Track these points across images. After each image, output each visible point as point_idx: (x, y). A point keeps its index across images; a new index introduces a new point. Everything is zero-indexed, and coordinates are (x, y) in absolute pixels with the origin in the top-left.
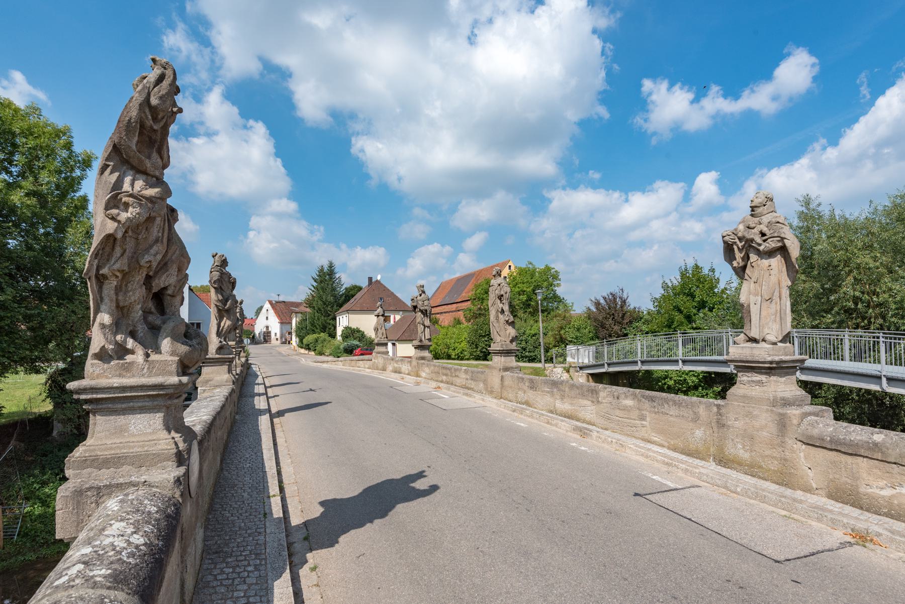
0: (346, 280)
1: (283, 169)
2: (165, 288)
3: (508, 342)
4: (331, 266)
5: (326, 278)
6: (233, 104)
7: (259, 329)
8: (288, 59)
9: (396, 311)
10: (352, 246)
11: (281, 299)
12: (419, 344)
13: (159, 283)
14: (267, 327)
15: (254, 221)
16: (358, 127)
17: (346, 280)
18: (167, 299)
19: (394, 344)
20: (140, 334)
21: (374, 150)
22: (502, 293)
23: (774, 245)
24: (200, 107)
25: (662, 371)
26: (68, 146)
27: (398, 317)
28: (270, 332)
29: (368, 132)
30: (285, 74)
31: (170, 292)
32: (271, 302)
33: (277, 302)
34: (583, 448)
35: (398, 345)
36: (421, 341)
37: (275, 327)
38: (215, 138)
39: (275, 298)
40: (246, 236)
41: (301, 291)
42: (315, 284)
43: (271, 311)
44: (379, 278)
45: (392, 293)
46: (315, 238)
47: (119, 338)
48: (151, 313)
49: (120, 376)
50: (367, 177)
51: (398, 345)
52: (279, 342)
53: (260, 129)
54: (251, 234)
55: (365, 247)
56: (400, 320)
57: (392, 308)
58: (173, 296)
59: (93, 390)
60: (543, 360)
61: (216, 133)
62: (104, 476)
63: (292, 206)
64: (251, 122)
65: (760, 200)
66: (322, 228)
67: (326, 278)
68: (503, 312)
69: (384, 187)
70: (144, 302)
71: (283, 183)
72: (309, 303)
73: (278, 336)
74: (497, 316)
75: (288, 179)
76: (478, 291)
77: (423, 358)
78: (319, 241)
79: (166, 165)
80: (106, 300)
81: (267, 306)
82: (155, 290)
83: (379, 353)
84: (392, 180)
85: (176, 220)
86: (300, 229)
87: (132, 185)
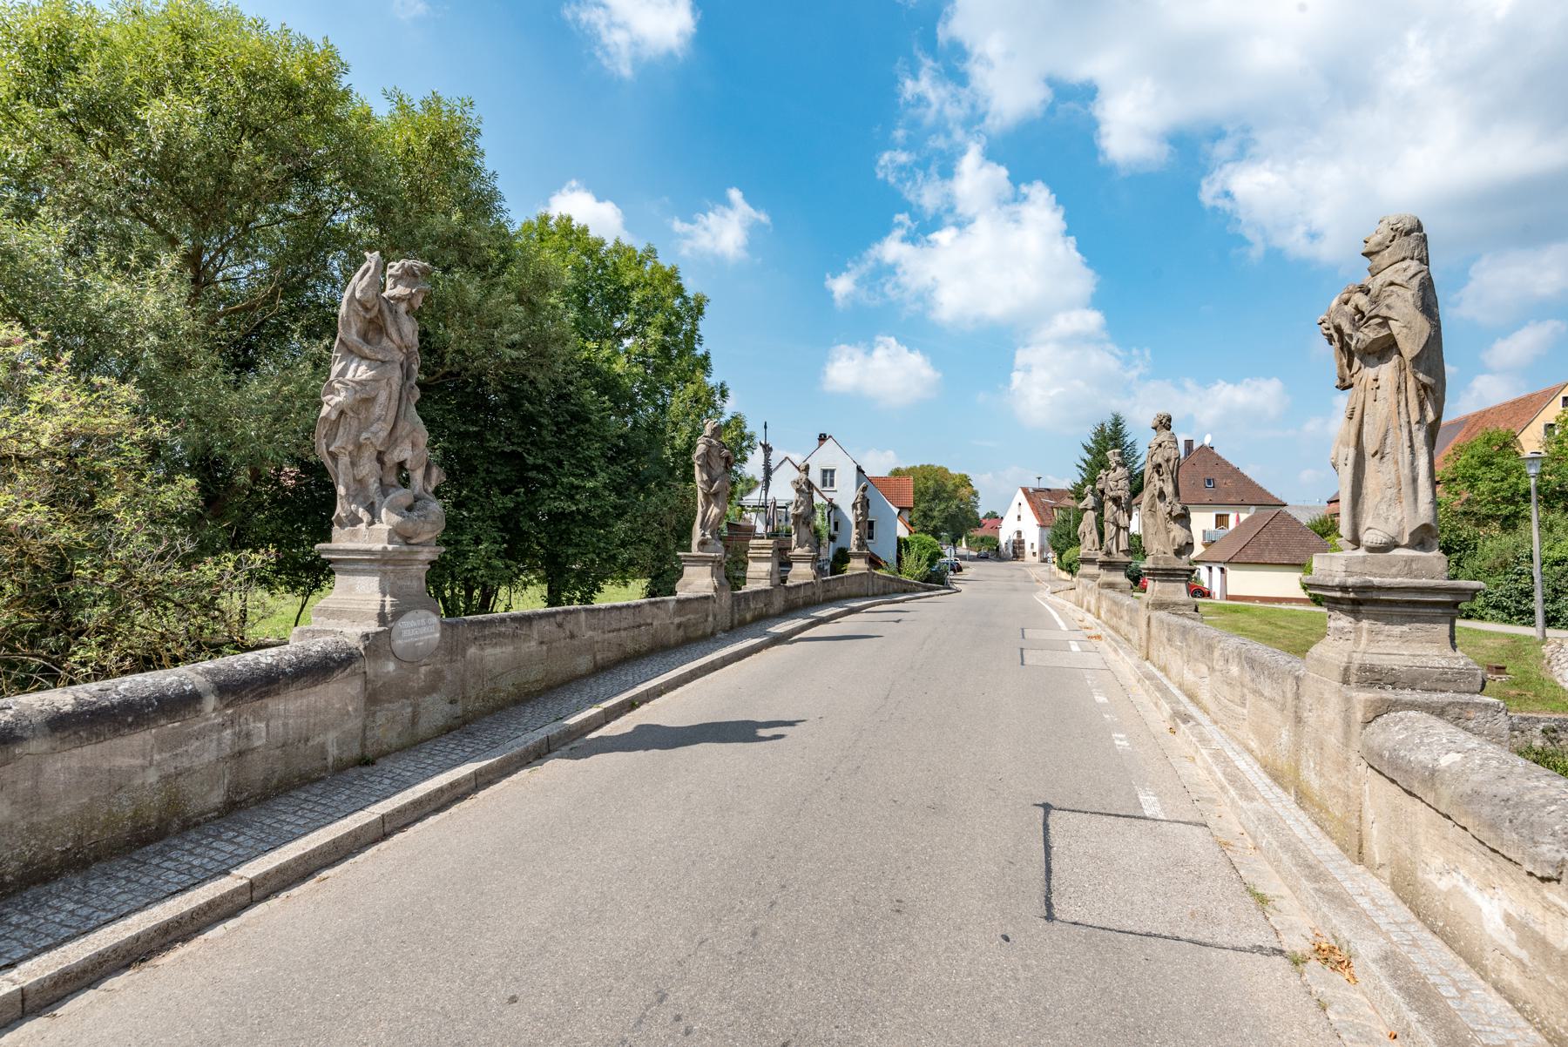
1: (1078, 255)
3: (1171, 554)
4: (1117, 422)
6: (999, 163)
7: (1005, 535)
8: (1096, 65)
9: (1242, 505)
10: (1206, 381)
11: (1043, 485)
12: (1105, 559)
14: (1019, 533)
15: (1022, 357)
16: (1223, 149)
19: (1222, 570)
21: (1252, 185)
22: (1160, 460)
23: (1372, 336)
24: (947, 182)
26: (679, 291)
27: (1244, 517)
28: (1022, 542)
29: (1242, 154)
30: (1088, 92)
32: (1025, 491)
33: (1036, 491)
35: (1230, 572)
36: (1109, 553)
37: (1032, 534)
38: (969, 228)
39: (1033, 484)
40: (1008, 381)
42: (1088, 457)
43: (1026, 506)
44: (1207, 441)
45: (1236, 470)
46: (1134, 373)
47: (353, 507)
50: (1242, 241)
51: (1230, 572)
52: (1037, 558)
53: (1040, 193)
54: (1017, 377)
55: (1235, 380)
56: (1247, 521)
57: (1232, 500)
60: (1539, 617)
61: (972, 221)
63: (1094, 319)
64: (1024, 189)
65: (1378, 238)
66: (1147, 353)
67: (1109, 441)
68: (1162, 495)
69: (1275, 256)
71: (1082, 282)
73: (1036, 549)
74: (1153, 505)
75: (1090, 273)
76: (1462, 461)
77: (1111, 586)
78: (1140, 377)
81: (1021, 497)
83: (1085, 576)
84: (1294, 243)
86: (1102, 360)
87: (356, 371)
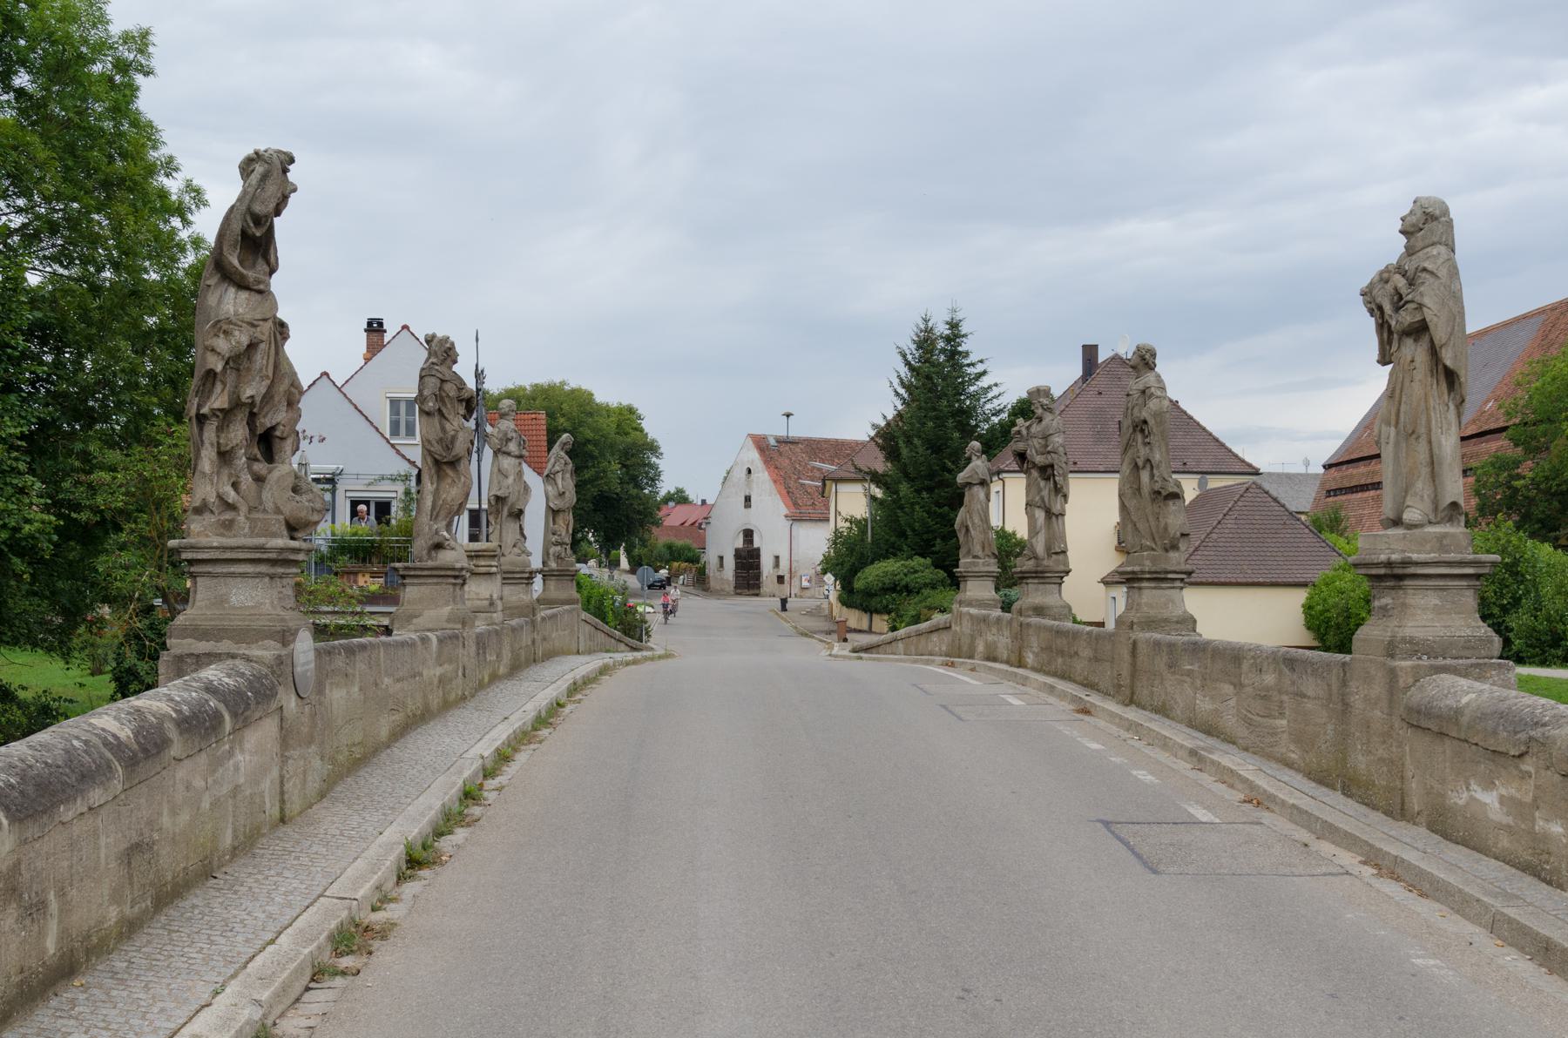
0: (1004, 380)
2: (273, 428)
5: (938, 375)
13: (266, 422)
17: (1004, 380)
18: (277, 444)
20: (243, 487)
25: (549, 532)
31: (278, 433)
33: (782, 441)
34: (1095, 746)
41: (863, 405)
48: (256, 460)
49: (222, 535)
58: (282, 439)
59: (192, 548)
62: (202, 647)
67: (938, 375)
70: (248, 446)
72: (888, 438)
79: (272, 271)
80: (207, 444)
82: (260, 431)
85: (285, 337)
